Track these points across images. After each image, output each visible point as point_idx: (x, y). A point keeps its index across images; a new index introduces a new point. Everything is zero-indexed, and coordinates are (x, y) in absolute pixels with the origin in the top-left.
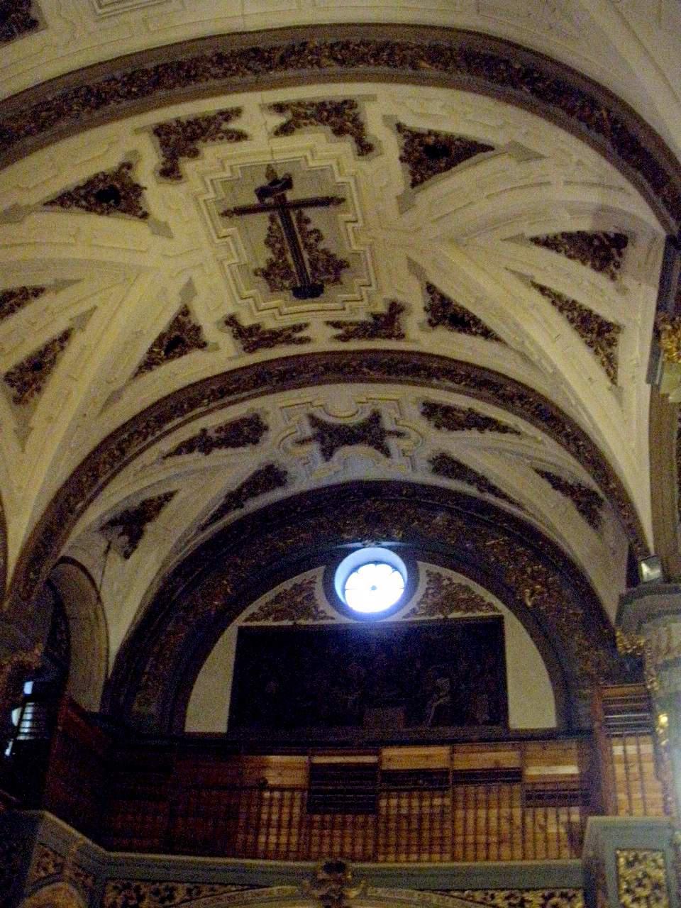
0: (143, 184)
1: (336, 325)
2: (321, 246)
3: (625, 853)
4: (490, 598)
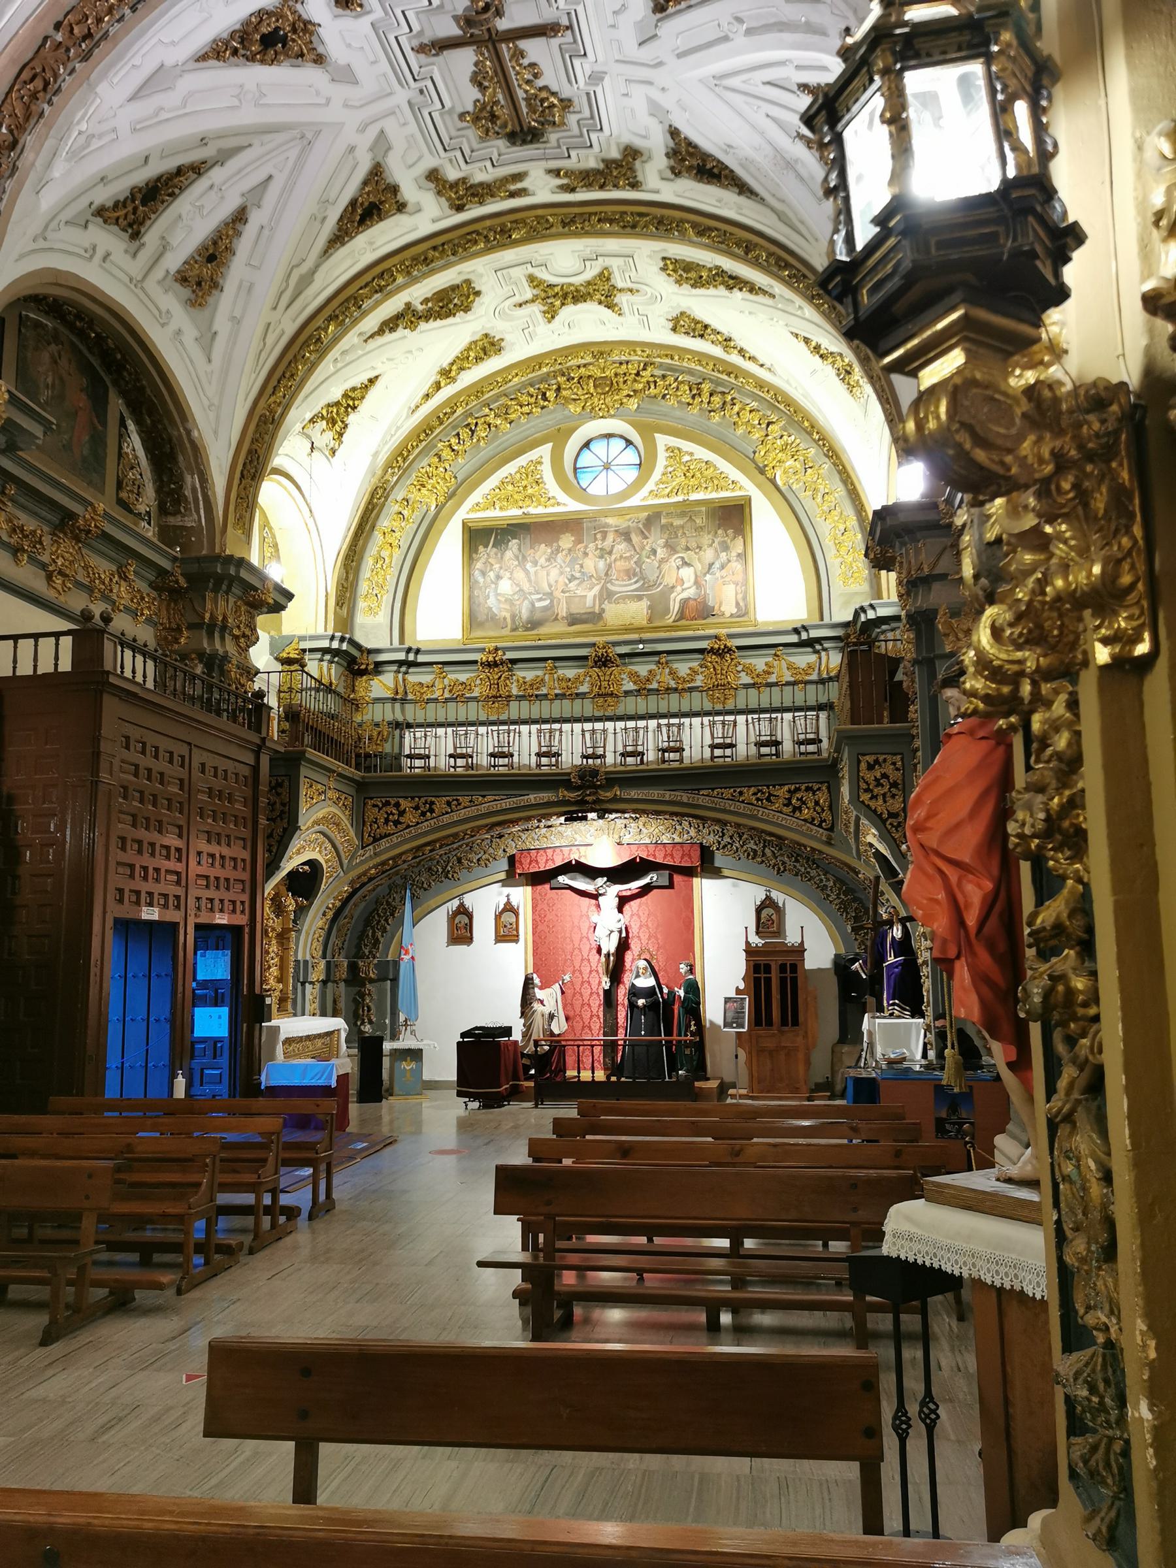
0: (316, 20)
1: (556, 173)
2: (540, 83)
3: (867, 758)
4: (733, 473)
